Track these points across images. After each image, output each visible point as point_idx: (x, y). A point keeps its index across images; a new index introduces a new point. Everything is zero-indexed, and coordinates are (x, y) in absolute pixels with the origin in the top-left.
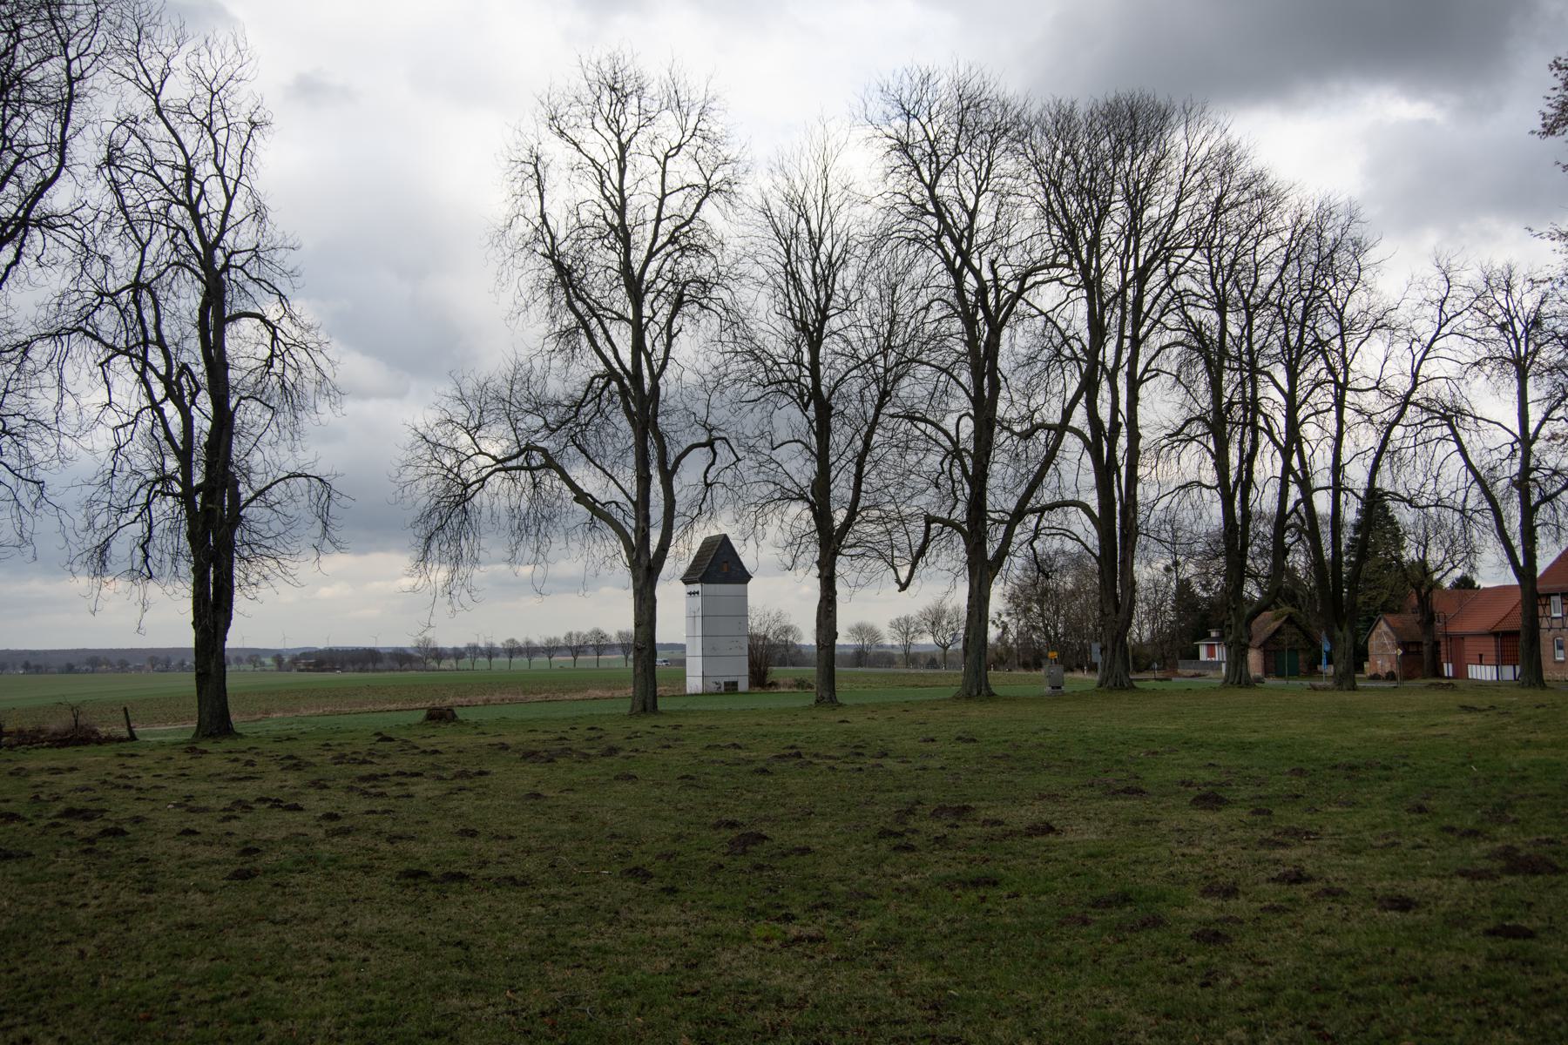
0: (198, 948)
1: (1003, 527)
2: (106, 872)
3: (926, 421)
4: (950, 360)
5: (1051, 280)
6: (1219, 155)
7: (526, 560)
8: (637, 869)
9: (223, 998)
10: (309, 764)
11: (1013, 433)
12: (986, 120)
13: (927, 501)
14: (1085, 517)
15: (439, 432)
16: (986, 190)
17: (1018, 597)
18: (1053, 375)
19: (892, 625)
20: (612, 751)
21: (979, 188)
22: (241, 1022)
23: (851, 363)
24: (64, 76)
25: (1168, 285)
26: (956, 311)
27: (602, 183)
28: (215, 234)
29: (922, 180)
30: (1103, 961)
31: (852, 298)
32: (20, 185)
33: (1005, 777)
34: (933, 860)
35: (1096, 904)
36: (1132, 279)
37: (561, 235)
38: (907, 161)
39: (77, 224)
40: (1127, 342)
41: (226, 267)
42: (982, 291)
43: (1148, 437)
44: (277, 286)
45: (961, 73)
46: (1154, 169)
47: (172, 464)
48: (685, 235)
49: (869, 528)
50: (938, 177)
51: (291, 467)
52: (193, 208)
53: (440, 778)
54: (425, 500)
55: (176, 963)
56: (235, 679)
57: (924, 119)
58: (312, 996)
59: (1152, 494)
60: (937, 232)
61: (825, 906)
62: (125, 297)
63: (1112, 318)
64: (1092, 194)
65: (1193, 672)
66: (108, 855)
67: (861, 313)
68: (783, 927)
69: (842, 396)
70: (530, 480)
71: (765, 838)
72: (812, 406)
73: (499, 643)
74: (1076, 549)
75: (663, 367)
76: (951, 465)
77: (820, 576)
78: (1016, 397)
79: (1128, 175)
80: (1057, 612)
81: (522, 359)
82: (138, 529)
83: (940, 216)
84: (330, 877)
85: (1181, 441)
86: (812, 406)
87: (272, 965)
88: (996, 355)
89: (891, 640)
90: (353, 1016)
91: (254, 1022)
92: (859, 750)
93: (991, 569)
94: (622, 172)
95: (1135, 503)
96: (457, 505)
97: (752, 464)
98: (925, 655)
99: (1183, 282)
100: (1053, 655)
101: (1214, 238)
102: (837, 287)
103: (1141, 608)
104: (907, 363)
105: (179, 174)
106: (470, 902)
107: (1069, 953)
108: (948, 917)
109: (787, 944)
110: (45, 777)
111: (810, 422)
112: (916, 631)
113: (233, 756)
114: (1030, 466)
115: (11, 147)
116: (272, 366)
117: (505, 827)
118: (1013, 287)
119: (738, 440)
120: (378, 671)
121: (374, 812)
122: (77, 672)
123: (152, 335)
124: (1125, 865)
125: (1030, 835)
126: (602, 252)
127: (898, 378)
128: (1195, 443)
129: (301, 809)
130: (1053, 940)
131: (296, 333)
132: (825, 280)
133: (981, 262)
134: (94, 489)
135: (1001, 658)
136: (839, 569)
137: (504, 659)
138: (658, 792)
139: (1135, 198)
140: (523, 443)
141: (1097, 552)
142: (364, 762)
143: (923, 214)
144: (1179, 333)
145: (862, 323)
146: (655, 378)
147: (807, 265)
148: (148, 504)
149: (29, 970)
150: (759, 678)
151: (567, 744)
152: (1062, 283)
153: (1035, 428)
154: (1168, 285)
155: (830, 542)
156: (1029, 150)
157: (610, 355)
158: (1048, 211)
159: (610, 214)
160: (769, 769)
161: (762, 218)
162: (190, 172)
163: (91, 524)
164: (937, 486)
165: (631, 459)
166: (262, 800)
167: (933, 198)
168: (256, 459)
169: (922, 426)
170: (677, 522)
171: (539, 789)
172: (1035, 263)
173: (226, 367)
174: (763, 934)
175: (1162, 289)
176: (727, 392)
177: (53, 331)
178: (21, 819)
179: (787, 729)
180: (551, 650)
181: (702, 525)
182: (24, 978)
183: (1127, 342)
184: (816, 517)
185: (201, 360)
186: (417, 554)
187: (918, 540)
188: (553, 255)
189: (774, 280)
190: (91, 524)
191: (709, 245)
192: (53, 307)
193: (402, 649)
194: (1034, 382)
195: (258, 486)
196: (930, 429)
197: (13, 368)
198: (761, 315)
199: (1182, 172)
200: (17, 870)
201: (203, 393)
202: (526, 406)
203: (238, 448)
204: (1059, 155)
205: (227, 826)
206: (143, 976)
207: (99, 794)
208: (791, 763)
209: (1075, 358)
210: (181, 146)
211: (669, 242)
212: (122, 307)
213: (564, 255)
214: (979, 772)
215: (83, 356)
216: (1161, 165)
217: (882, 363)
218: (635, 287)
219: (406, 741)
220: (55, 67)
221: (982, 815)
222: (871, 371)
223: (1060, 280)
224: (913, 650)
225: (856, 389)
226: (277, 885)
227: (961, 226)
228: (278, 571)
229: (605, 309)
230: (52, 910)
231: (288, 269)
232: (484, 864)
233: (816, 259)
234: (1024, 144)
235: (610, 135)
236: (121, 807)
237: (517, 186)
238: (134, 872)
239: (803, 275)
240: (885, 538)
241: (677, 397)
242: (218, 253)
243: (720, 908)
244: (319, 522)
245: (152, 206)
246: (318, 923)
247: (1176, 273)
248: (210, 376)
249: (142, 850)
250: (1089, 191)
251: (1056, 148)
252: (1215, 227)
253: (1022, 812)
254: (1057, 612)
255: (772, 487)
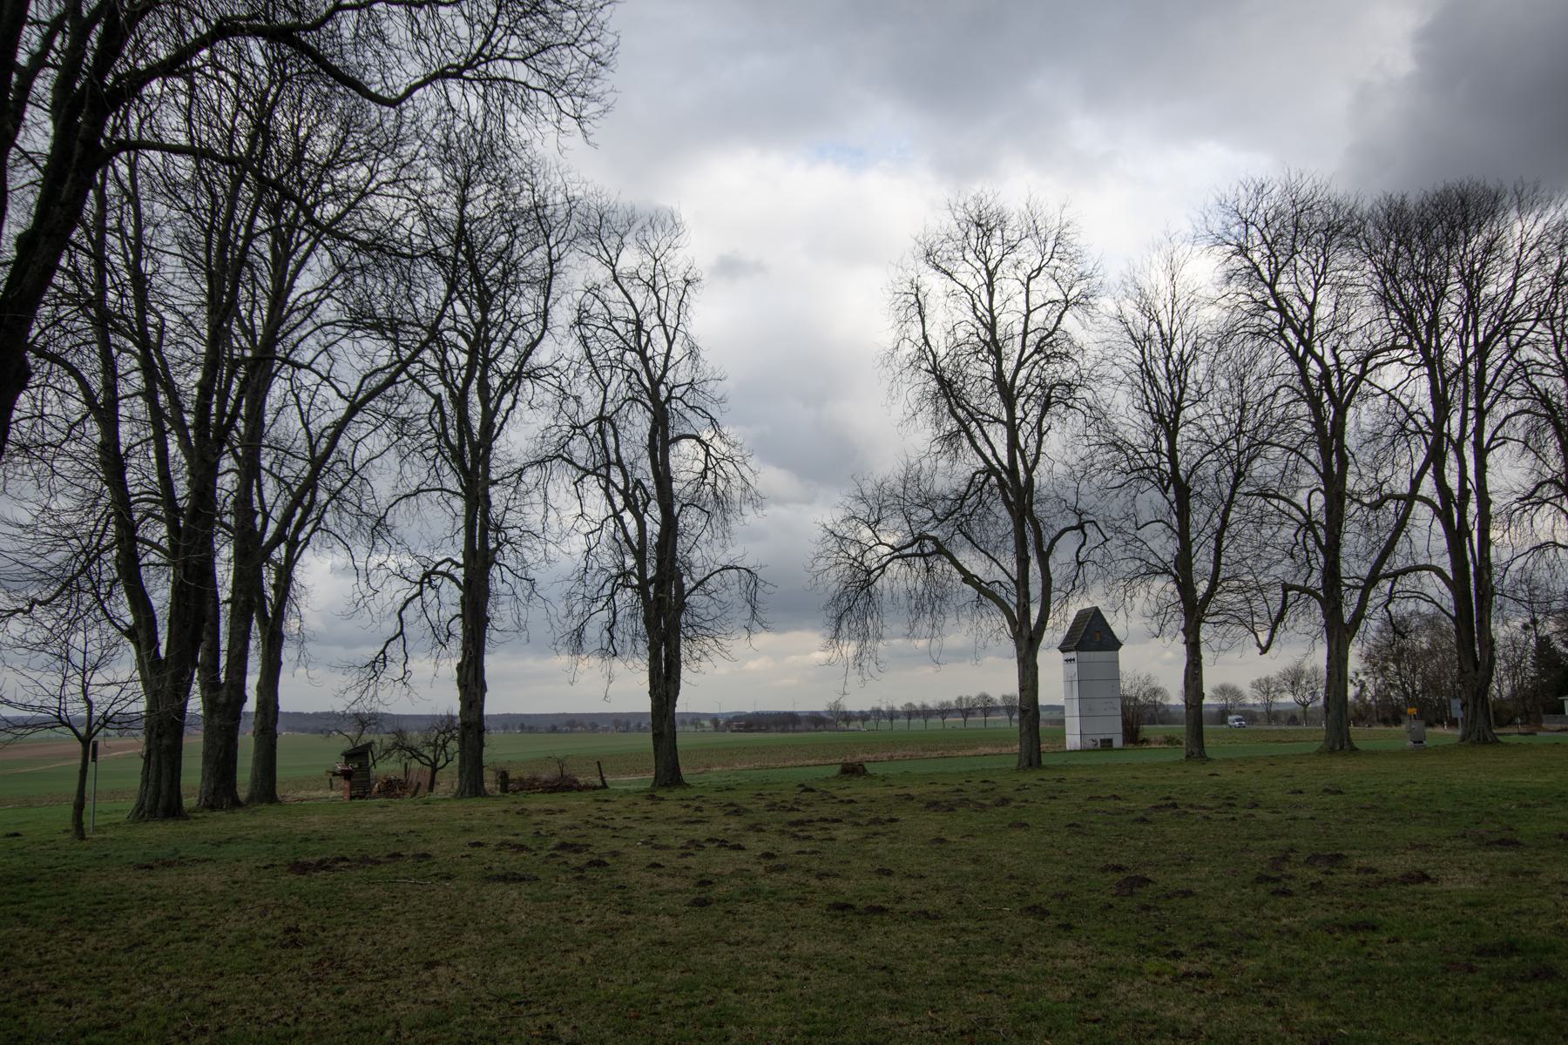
0: (670, 962)
1: (1358, 592)
2: (595, 896)
3: (1280, 498)
4: (1298, 440)
5: (1392, 361)
6: (1556, 229)
7: (924, 634)
8: (1035, 907)
9: (694, 1005)
10: (746, 810)
11: (1363, 504)
12: (1319, 220)
13: (1284, 570)
14: (1438, 580)
15: (845, 529)
16: (1324, 283)
17: (1374, 657)
18: (1399, 449)
19: (1253, 685)
20: (1005, 801)
21: (1317, 282)
22: (709, 1025)
23: (1206, 449)
24: (547, 260)
25: (1511, 357)
26: (1302, 396)
27: (974, 306)
28: (659, 373)
29: (1262, 279)
30: (1495, 1009)
31: (1204, 390)
32: (516, 347)
33: (1374, 827)
34: (1311, 904)
35: (1481, 952)
36: (1473, 355)
37: (942, 352)
38: (1247, 263)
39: (556, 374)
40: (1471, 414)
41: (669, 399)
42: (1326, 375)
43: (1498, 502)
44: (709, 411)
45: (1293, 180)
46: (1488, 249)
47: (630, 562)
48: (1050, 344)
49: (1230, 597)
50: (1277, 276)
51: (724, 561)
52: (642, 353)
53: (857, 824)
54: (835, 586)
55: (654, 973)
56: (685, 738)
57: (1261, 225)
58: (765, 1007)
59: (1506, 556)
60: (1280, 325)
61: (1210, 945)
62: (592, 428)
63: (1454, 393)
64: (1427, 279)
65: (1558, 726)
66: (595, 882)
67: (1213, 402)
68: (1172, 963)
69: (1199, 478)
70: (924, 565)
71: (1149, 881)
72: (1171, 489)
73: (899, 706)
74: (1431, 610)
75: (1036, 461)
76: (1305, 537)
77: (1186, 643)
78: (1364, 471)
79: (1462, 257)
80: (1414, 670)
81: (913, 461)
82: (605, 615)
83: (1281, 310)
84: (771, 907)
85: (1533, 504)
86: (1171, 489)
87: (730, 980)
88: (1343, 433)
89: (1252, 699)
90: (800, 1026)
91: (720, 1026)
92: (1231, 801)
93: (1348, 632)
94: (991, 294)
95: (1489, 566)
96: (862, 589)
97: (1119, 543)
98: (1285, 713)
99: (1526, 353)
100: (1412, 711)
101: (1556, 308)
102: (1189, 381)
103: (1500, 665)
104: (1258, 445)
105: (631, 327)
106: (891, 932)
107: (1457, 1000)
108: (1331, 958)
109: (1177, 979)
110: (542, 817)
111: (1170, 503)
112: (1277, 690)
113: (685, 803)
114: (1381, 535)
115: (509, 319)
116: (706, 477)
117: (916, 867)
118: (1356, 370)
119: (1105, 522)
120: (798, 731)
121: (804, 852)
122: (559, 732)
123: (613, 457)
124: (1507, 914)
125: (1405, 883)
126: (977, 365)
127: (1249, 461)
128: (1548, 505)
129: (742, 849)
130: (1439, 986)
131: (724, 449)
132: (1177, 375)
133: (1323, 349)
134: (572, 584)
135: (1360, 715)
136: (1203, 636)
137: (904, 721)
138: (1048, 839)
139: (1471, 277)
140: (916, 532)
141: (1453, 613)
142: (792, 809)
143: (1265, 310)
144: (1524, 401)
145: (1214, 412)
146: (1029, 471)
147: (1161, 363)
148: (612, 595)
149: (546, 971)
150: (1132, 735)
151: (964, 795)
152: (1403, 363)
153: (1384, 499)
154: (1511, 357)
155: (1194, 612)
156: (1363, 243)
157: (988, 453)
158: (1384, 298)
159: (982, 331)
160: (1149, 818)
161: (1114, 323)
162: (639, 325)
163: (570, 612)
164: (1292, 556)
165: (1011, 543)
166: (710, 840)
167: (1274, 295)
168: (696, 556)
169: (1275, 502)
170: (1054, 596)
171: (943, 835)
172: (1375, 346)
173: (671, 480)
174: (1155, 969)
175: (1505, 362)
176: (1094, 480)
177: (539, 459)
178: (529, 850)
179: (1163, 782)
180: (944, 712)
181: (1076, 598)
182: (541, 977)
183: (1471, 414)
184: (1179, 588)
185: (651, 475)
186: (829, 632)
187: (1276, 606)
188: (936, 371)
189: (1132, 379)
190: (570, 612)
191: (1072, 352)
192: (539, 439)
193: (817, 713)
194: (1381, 456)
195: (698, 578)
196: (1282, 505)
197: (511, 490)
198: (1122, 410)
199: (1517, 250)
200: (529, 890)
201: (652, 502)
202: (917, 501)
203: (682, 544)
204: (1392, 245)
205: (685, 862)
206: (630, 981)
207: (583, 832)
208: (1168, 813)
209: (1419, 431)
210: (632, 304)
211: (1035, 352)
212: (591, 436)
213: (943, 370)
214: (1347, 822)
215: (561, 483)
216: (1494, 246)
217: (1235, 447)
218: (1008, 394)
219: (824, 792)
220: (540, 254)
221: (1356, 863)
222: (1225, 454)
223: (1401, 360)
224: (1273, 708)
225: (1211, 471)
226: (729, 912)
227: (1302, 318)
228: (716, 648)
229: (983, 414)
230: (557, 924)
231: (717, 397)
232: (900, 899)
233: (1169, 356)
234: (1358, 238)
235: (979, 264)
236: (603, 844)
237: (902, 314)
238: (616, 897)
239: (1158, 372)
240: (1245, 606)
241: (1050, 487)
242: (662, 387)
243: (1112, 944)
244: (749, 606)
245: (612, 354)
246: (764, 946)
247: (1519, 345)
248: (658, 488)
249: (620, 878)
250: (1425, 277)
251: (1389, 240)
252: (1556, 298)
253: (1396, 861)
254: (1414, 670)
255: (1138, 563)
